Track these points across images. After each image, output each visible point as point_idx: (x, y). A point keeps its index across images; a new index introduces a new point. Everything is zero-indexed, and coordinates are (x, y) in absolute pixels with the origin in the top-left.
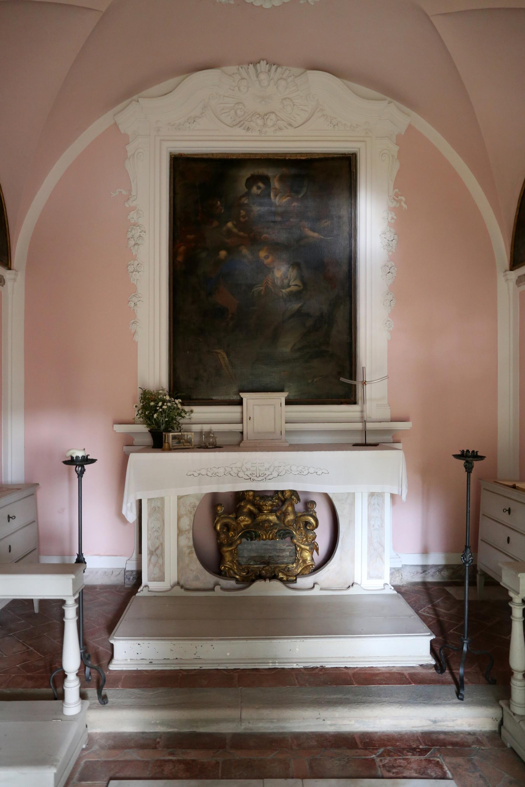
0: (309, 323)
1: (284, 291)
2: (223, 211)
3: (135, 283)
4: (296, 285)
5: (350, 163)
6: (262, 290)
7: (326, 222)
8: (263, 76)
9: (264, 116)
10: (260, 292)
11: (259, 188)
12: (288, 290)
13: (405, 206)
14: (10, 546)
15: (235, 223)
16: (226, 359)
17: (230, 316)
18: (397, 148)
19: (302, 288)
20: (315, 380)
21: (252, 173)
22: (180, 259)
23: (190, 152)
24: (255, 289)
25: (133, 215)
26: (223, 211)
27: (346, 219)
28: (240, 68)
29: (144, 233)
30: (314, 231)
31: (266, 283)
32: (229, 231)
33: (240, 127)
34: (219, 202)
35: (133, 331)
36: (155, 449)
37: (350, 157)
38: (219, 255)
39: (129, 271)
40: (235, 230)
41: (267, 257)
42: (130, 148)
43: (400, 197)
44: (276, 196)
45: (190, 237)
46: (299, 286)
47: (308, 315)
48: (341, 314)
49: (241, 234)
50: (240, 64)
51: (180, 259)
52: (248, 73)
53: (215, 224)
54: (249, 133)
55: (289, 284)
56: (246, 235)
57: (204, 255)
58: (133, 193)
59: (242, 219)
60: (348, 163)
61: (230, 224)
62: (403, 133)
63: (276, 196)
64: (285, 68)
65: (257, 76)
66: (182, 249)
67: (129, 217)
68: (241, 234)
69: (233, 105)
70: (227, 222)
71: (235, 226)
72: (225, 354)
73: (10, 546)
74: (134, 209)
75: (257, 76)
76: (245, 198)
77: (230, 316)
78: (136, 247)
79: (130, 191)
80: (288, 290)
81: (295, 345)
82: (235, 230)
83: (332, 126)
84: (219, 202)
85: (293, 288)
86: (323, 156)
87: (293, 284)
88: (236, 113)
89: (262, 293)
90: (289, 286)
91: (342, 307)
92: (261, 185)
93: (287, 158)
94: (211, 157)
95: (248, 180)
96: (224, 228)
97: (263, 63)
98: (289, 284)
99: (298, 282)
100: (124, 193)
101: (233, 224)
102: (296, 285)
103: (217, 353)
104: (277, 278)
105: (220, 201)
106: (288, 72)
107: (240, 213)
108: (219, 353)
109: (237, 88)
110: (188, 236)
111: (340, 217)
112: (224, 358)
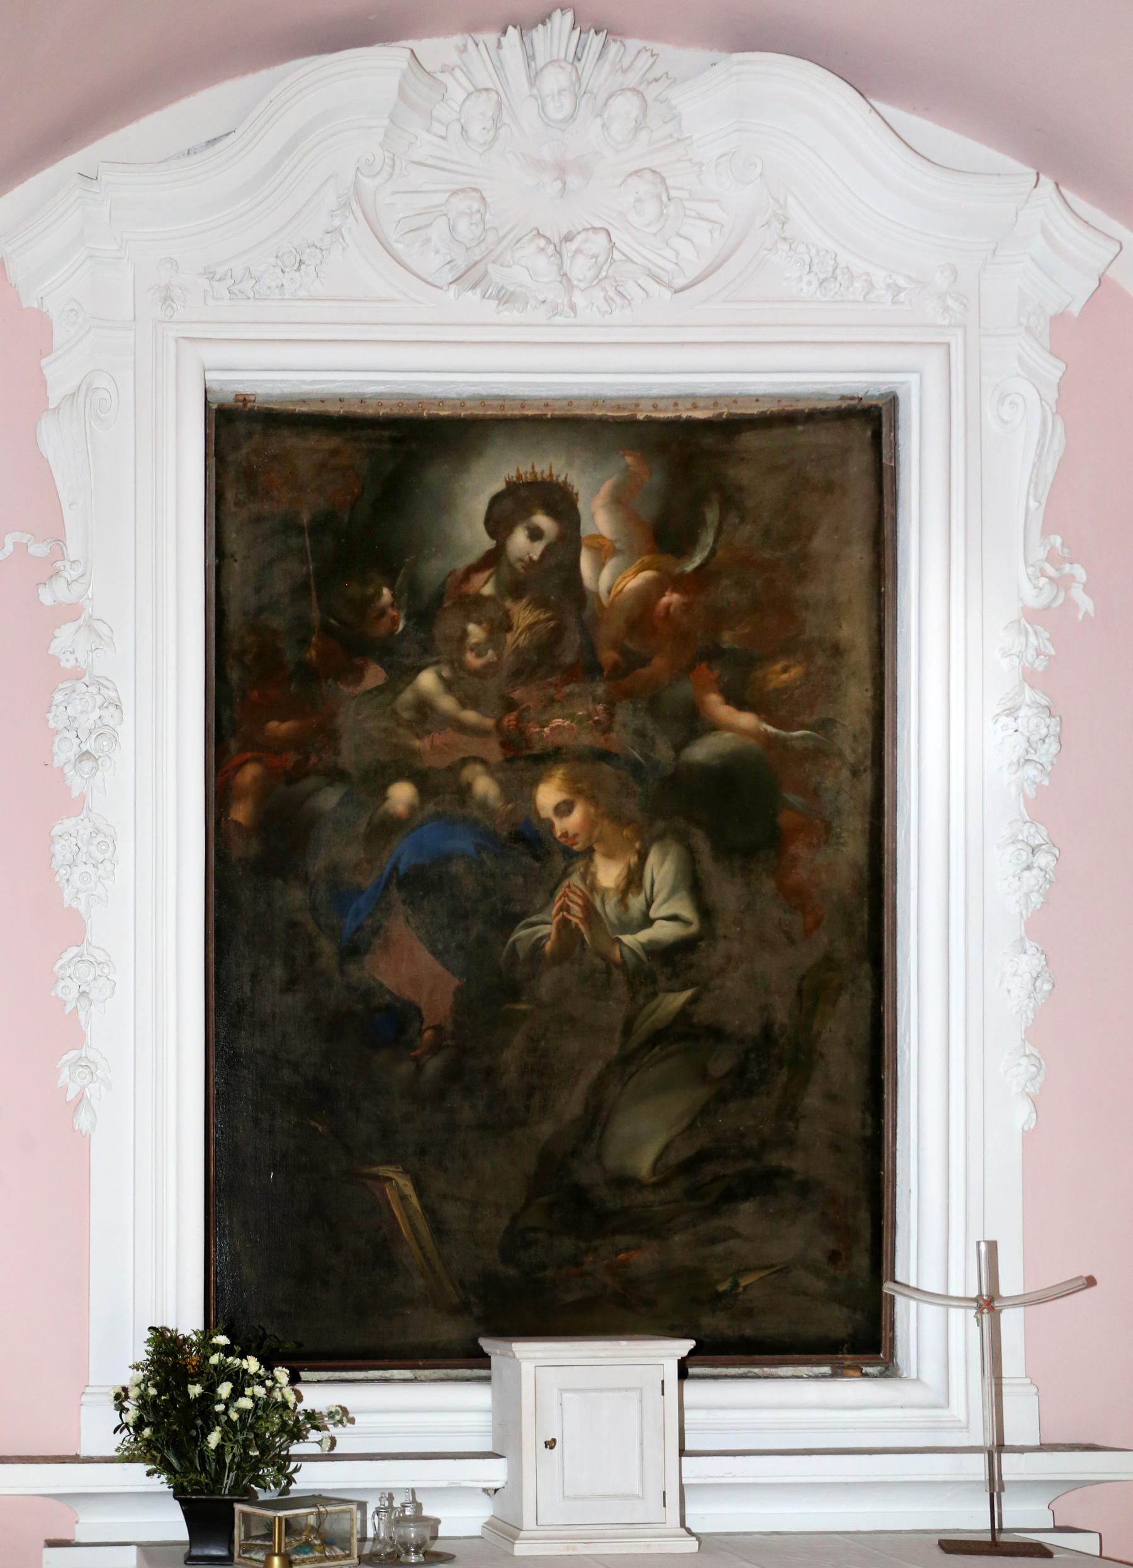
0: (722, 1064)
1: (627, 939)
2: (401, 627)
3: (82, 908)
4: (673, 918)
5: (877, 436)
6: (548, 936)
7: (785, 670)
8: (554, 80)
9: (559, 245)
10: (537, 946)
11: (535, 534)
12: (644, 936)
13: (1086, 604)
15: (446, 673)
16: (414, 1200)
17: (428, 1035)
18: (1054, 370)
20: (744, 1282)
21: (525, 469)
22: (241, 813)
23: (276, 390)
25: (67, 642)
27: (860, 656)
28: (471, 46)
29: (117, 713)
30: (741, 705)
32: (424, 707)
33: (474, 287)
35: (70, 1096)
36: (885, 1343)
37: (878, 409)
38: (385, 799)
39: (59, 857)
40: (447, 703)
41: (563, 809)
42: (61, 374)
43: (1067, 568)
45: (278, 728)
46: (687, 923)
47: (716, 1034)
48: (836, 1031)
49: (470, 716)
50: (472, 27)
51: (241, 813)
52: (499, 67)
53: (375, 676)
54: (509, 315)
55: (646, 914)
56: (489, 723)
57: (329, 799)
58: (73, 549)
60: (869, 433)
61: (427, 680)
62: (1076, 309)
64: (634, 44)
65: (534, 78)
66: (250, 773)
67: (55, 647)
68: (470, 716)
69: (443, 197)
70: (419, 670)
71: (449, 686)
72: (409, 1184)
74: (71, 612)
75: (534, 78)
77: (428, 1035)
78: (87, 765)
79: (59, 541)
80: (644, 936)
81: (667, 1147)
82: (447, 703)
83: (815, 284)
85: (663, 931)
86: (774, 407)
87: (665, 911)
88: (452, 229)
89: (548, 946)
90: (647, 922)
91: (844, 1001)
92: (542, 520)
93: (641, 416)
94: (359, 410)
95: (513, 489)
96: (407, 696)
97: (562, 21)
98: (646, 914)
100: (38, 550)
102: (673, 918)
103: (376, 1177)
104: (606, 890)
105: (391, 587)
106: (645, 60)
107: (465, 634)
108: (390, 1179)
109: (457, 127)
110: (273, 725)
111: (837, 651)
112: (403, 1198)
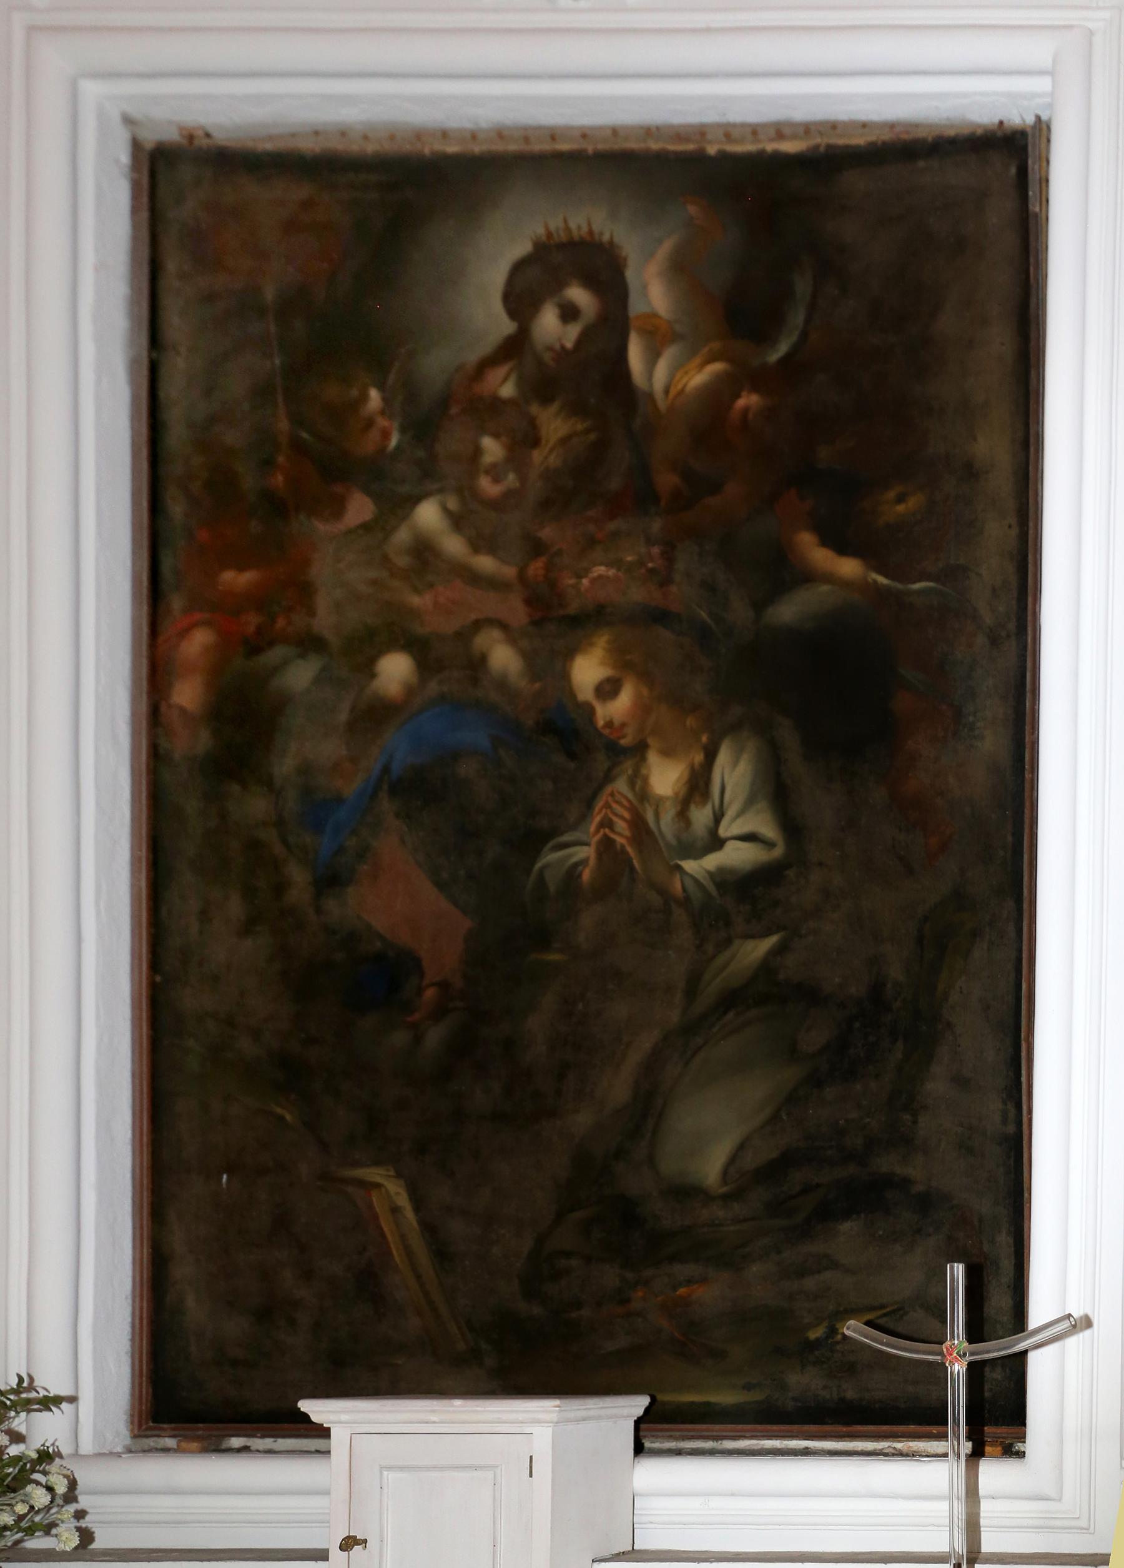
0: (816, 1036)
1: (689, 865)
2: (394, 441)
4: (750, 838)
6: (584, 862)
10: (572, 873)
14: (531, 1457)
15: (453, 504)
19: (778, 852)
21: (555, 223)
22: (187, 694)
24: (550, 857)
26: (394, 441)
31: (601, 825)
32: (424, 551)
34: (374, 394)
38: (373, 676)
40: (454, 545)
41: (607, 690)
44: (653, 356)
45: (237, 579)
46: (769, 844)
47: (809, 995)
49: (485, 563)
53: (360, 508)
55: (713, 832)
59: (488, 487)
60: (1013, 170)
61: (428, 514)
63: (653, 356)
68: (485, 563)
70: (415, 500)
71: (457, 521)
73: (531, 1457)
76: (501, 371)
77: (430, 994)
81: (741, 1147)
82: (454, 545)
84: (374, 394)
85: (736, 856)
87: (738, 828)
89: (587, 875)
90: (716, 843)
92: (578, 295)
93: (712, 150)
94: (338, 145)
96: (402, 536)
98: (713, 832)
99: (762, 823)
101: (445, 510)
102: (750, 838)
105: (381, 387)
108: (378, 1186)
111: (971, 472)
